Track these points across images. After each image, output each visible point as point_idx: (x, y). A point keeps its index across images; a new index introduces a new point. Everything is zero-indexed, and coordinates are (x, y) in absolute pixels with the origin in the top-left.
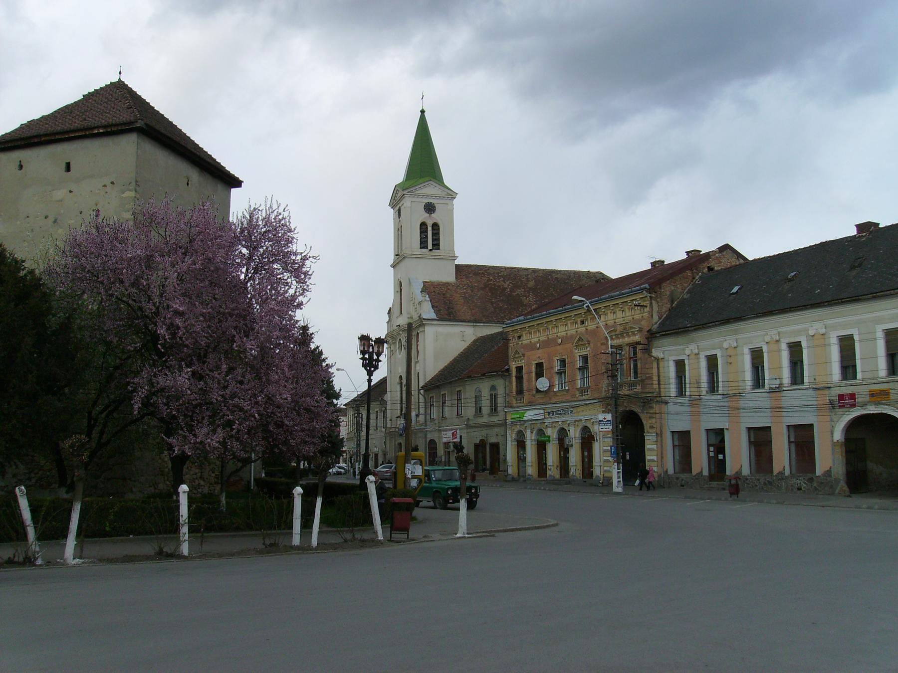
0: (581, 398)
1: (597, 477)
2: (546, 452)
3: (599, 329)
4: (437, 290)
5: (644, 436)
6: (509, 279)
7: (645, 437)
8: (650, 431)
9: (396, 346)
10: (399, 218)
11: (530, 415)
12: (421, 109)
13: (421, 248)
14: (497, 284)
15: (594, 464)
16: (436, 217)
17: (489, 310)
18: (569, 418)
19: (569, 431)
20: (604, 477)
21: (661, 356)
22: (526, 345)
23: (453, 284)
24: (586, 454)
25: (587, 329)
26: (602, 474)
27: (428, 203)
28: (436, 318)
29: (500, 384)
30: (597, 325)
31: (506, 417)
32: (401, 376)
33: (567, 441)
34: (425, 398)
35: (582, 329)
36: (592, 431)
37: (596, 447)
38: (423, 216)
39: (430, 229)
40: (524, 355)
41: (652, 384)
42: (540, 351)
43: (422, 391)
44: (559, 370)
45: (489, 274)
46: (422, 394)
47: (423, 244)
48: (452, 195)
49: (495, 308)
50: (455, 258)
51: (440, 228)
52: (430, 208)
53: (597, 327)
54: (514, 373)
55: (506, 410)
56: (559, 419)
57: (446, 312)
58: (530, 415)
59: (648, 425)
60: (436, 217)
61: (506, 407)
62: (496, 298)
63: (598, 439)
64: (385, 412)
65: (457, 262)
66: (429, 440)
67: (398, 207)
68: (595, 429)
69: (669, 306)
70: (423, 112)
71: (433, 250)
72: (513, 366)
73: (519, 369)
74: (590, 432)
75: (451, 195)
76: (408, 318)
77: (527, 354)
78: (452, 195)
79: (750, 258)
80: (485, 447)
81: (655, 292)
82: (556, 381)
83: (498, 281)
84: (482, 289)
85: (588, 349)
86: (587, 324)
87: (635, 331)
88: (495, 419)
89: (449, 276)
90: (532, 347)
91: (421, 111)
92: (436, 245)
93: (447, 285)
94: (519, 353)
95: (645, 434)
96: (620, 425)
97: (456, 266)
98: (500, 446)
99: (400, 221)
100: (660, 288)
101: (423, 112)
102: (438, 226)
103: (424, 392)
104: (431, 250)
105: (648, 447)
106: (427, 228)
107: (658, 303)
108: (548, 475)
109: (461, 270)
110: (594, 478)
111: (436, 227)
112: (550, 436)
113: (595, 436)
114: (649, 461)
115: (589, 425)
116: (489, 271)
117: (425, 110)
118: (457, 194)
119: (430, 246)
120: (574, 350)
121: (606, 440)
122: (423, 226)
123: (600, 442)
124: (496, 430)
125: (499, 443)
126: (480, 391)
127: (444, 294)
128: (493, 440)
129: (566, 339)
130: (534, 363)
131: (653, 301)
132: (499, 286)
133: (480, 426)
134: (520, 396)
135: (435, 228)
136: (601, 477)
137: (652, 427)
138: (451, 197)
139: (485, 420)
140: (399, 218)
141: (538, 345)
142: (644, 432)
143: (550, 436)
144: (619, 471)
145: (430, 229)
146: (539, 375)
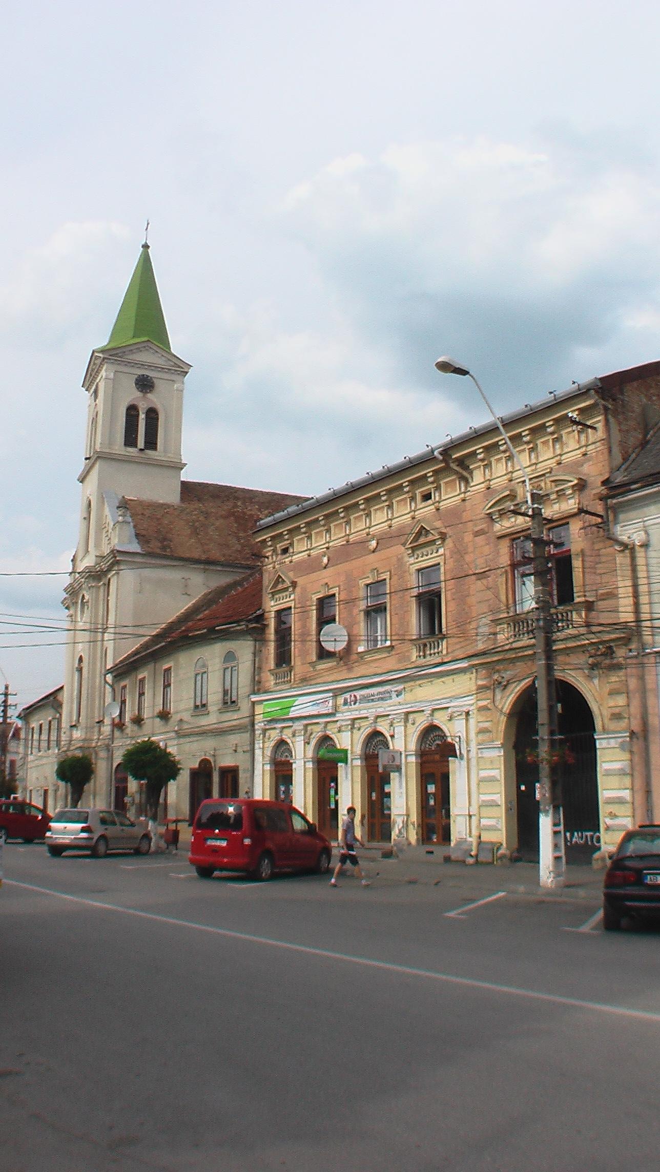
0: (422, 661)
1: (461, 842)
2: (337, 784)
3: (467, 503)
4: (147, 513)
5: (595, 740)
6: (267, 508)
7: (597, 742)
8: (612, 725)
9: (76, 608)
10: (95, 401)
11: (303, 706)
12: (143, 243)
13: (125, 445)
14: (249, 513)
15: (454, 810)
16: (154, 399)
17: (233, 547)
18: (394, 705)
19: (392, 736)
20: (480, 843)
21: (638, 538)
22: (300, 563)
23: (176, 507)
24: (431, 789)
25: (438, 509)
26: (475, 832)
27: (143, 375)
28: (139, 551)
29: (244, 649)
30: (462, 496)
31: (254, 711)
32: (81, 656)
33: (383, 760)
34: (114, 690)
35: (425, 510)
36: (448, 734)
37: (458, 773)
38: (130, 394)
39: (142, 416)
40: (294, 584)
41: (616, 611)
42: (330, 570)
43: (109, 678)
44: (370, 606)
45: (237, 498)
46: (109, 685)
47: (130, 440)
48: (182, 368)
49: (243, 546)
50: (180, 467)
51: (160, 417)
52: (145, 385)
53: (464, 500)
54: (272, 624)
55: (254, 698)
56: (370, 710)
57: (160, 545)
58: (303, 706)
59: (606, 713)
60: (154, 399)
61: (254, 693)
62: (245, 531)
63: (464, 752)
64: (59, 721)
65: (187, 475)
66: (117, 764)
67: (95, 383)
68: (454, 730)
69: (641, 436)
70: (146, 247)
71: (147, 451)
72: (271, 606)
73: (282, 614)
74: (444, 736)
75: (180, 369)
76: (96, 556)
77: (301, 581)
78: (182, 368)
79: (294, 805)
80: (209, 775)
81: (614, 400)
82: (361, 628)
83: (249, 508)
84: (225, 517)
85: (441, 551)
86: (437, 499)
87: (568, 488)
88: (233, 718)
89: (171, 496)
90: (311, 565)
91: (143, 246)
92: (151, 443)
93: (165, 506)
94: (283, 581)
95: (596, 737)
96: (559, 705)
97: (183, 483)
98: (241, 773)
99: (96, 404)
100: (622, 394)
101: (146, 247)
102: (157, 414)
103: (113, 680)
104: (141, 450)
105: (606, 766)
106: (138, 414)
107: (620, 424)
108: (392, 840)
109: (189, 490)
110: (452, 844)
111: (152, 415)
112: (347, 750)
113: (457, 747)
114: (610, 801)
115: (440, 720)
116: (236, 495)
117: (149, 244)
118: (191, 366)
119: (141, 442)
120: (406, 559)
121: (488, 754)
122: (132, 411)
123: (469, 760)
124: (234, 739)
125: (238, 767)
126: (204, 666)
127: (158, 519)
128: (227, 761)
129: (384, 540)
130: (315, 598)
131: (610, 417)
132: (252, 516)
133: (203, 733)
134: (285, 668)
135: (153, 415)
136: (473, 840)
137: (617, 717)
138: (182, 370)
139: (211, 720)
140: (95, 401)
141: (325, 560)
142: (594, 730)
143: (347, 750)
144: (557, 829)
145: (142, 416)
146: (325, 620)
